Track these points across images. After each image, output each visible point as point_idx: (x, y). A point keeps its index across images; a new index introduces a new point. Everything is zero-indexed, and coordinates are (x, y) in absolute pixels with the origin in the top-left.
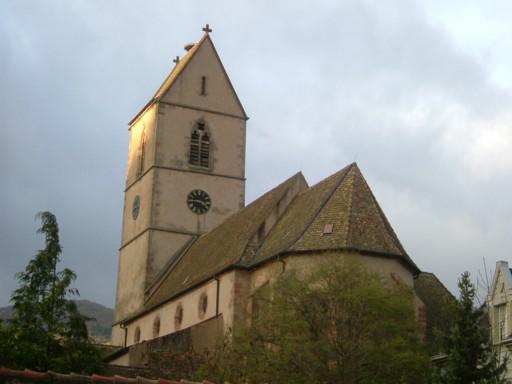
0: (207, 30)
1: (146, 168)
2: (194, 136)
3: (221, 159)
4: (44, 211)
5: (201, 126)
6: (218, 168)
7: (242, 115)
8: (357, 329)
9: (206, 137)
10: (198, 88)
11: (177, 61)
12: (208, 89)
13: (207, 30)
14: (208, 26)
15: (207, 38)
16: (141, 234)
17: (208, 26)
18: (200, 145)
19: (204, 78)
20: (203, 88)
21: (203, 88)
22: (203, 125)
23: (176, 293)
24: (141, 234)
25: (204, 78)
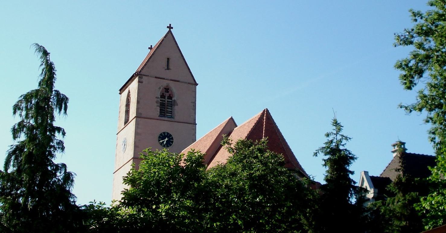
0: (170, 27)
1: (130, 119)
2: (163, 96)
3: (179, 111)
4: (36, 43)
5: (167, 89)
6: (177, 118)
7: (193, 82)
8: (440, 4)
9: (170, 97)
10: (164, 63)
11: (151, 48)
12: (171, 66)
13: (170, 27)
14: (170, 25)
15: (170, 32)
16: (129, 161)
17: (170, 25)
18: (166, 102)
19: (168, 59)
20: (168, 62)
21: (168, 62)
22: (168, 89)
23: (186, 124)
24: (129, 161)
25: (168, 59)
